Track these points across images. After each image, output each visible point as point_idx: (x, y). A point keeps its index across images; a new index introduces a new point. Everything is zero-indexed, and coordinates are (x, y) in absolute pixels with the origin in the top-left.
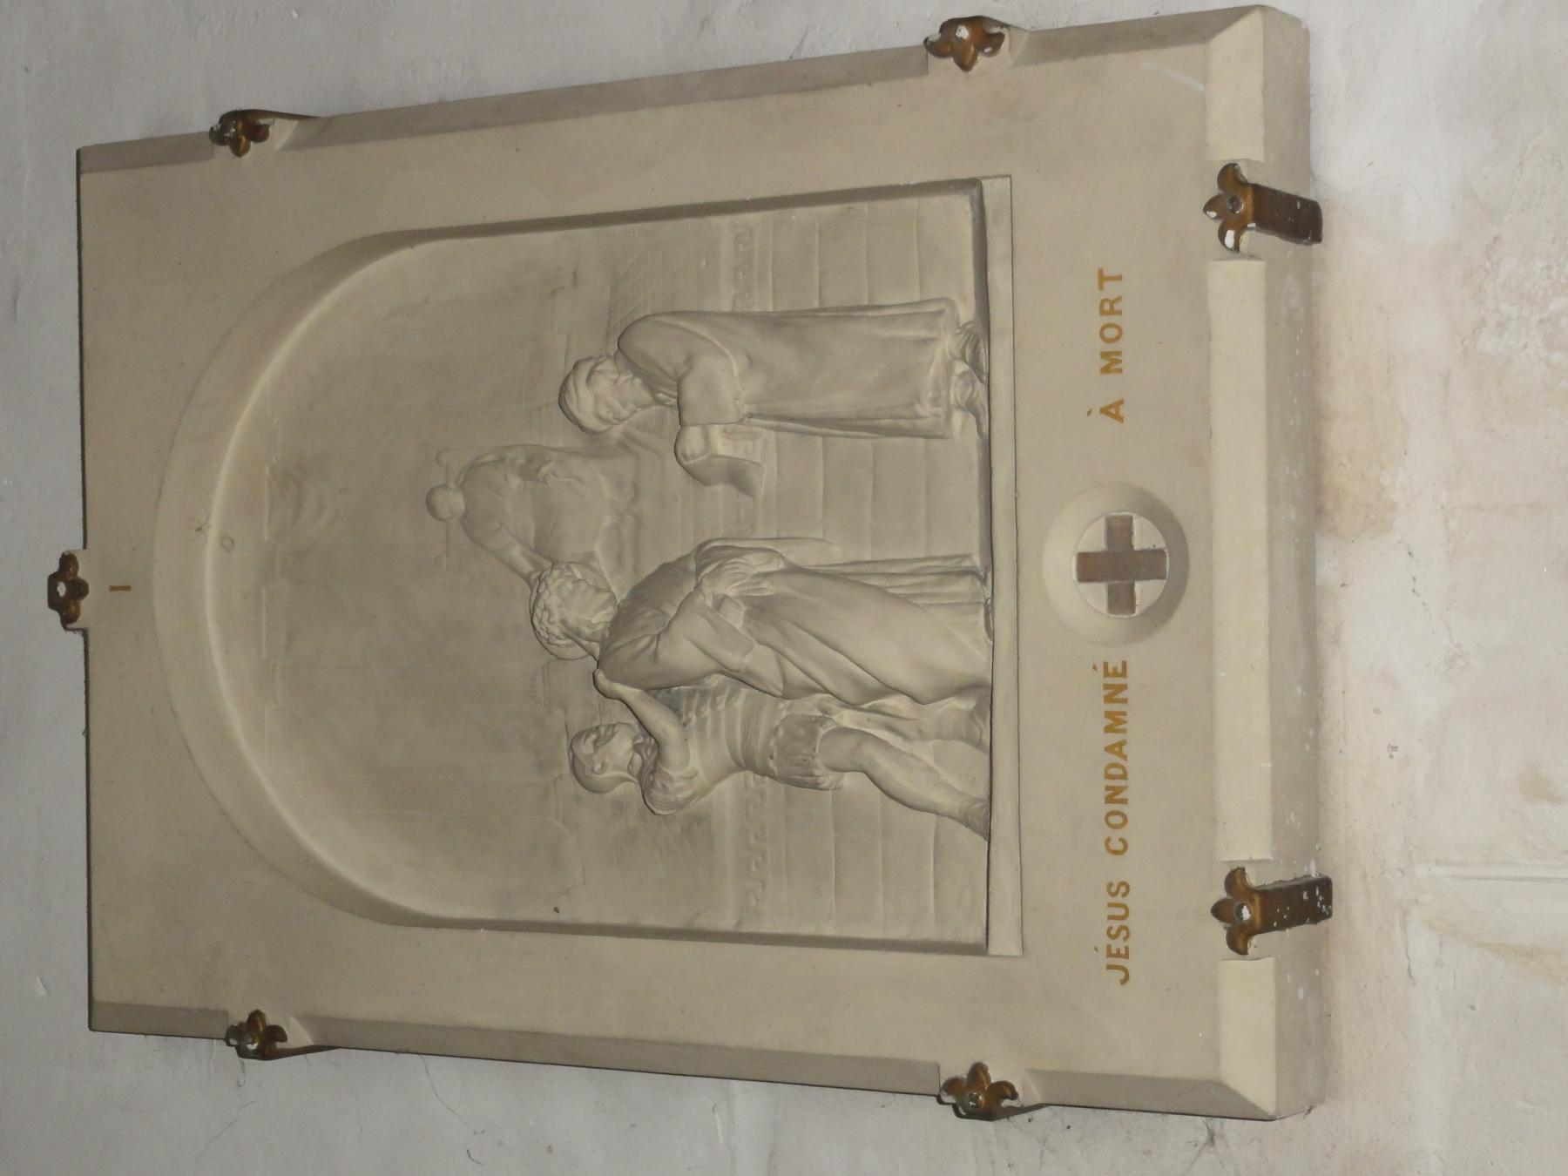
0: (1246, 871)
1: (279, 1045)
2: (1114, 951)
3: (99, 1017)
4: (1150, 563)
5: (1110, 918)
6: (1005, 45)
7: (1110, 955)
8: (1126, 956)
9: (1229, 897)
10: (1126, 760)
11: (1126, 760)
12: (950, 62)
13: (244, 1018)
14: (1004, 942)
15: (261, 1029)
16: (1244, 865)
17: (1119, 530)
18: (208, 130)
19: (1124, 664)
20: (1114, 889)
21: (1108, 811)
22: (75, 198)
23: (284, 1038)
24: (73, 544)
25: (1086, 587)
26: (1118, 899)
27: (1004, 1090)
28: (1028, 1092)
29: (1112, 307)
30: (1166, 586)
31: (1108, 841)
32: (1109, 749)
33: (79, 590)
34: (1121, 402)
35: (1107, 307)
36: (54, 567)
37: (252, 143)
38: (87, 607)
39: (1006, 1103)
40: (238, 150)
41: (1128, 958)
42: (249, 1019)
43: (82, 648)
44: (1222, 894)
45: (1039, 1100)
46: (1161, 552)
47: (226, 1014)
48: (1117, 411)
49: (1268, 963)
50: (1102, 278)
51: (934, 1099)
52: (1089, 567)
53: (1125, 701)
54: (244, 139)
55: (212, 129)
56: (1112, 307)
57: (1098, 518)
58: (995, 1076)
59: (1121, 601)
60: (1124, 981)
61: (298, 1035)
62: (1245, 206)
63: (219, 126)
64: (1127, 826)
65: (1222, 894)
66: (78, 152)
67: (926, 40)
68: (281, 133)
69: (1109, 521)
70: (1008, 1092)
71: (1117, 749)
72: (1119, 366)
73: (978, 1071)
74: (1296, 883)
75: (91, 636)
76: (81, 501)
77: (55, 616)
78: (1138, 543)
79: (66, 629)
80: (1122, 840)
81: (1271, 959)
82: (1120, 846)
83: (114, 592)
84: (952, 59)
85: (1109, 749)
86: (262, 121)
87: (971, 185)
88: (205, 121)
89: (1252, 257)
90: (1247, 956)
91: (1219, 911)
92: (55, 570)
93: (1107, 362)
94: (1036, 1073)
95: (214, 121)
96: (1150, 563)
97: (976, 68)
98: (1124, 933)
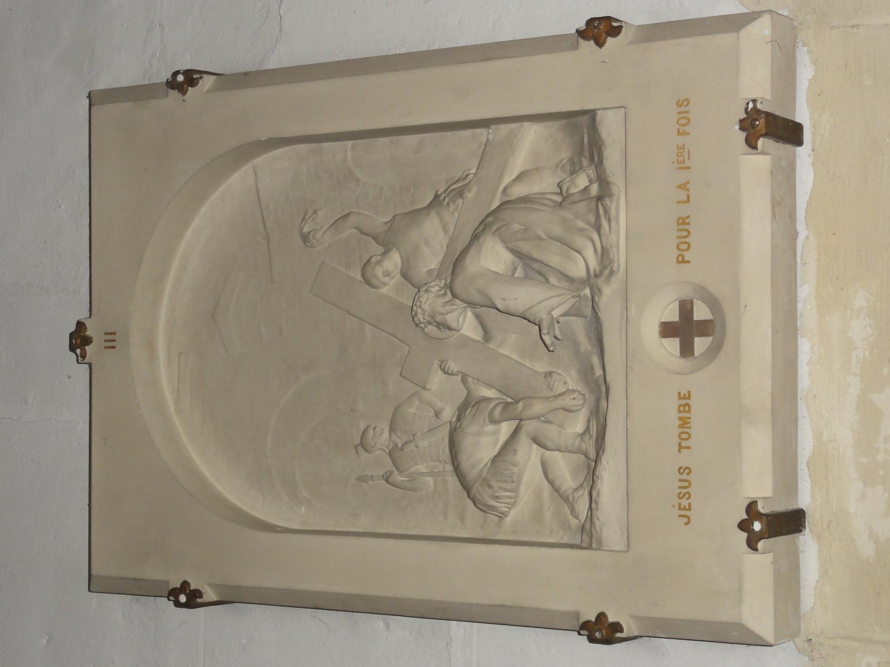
0: (758, 503)
1: (199, 600)
2: (679, 161)
3: (94, 584)
4: (705, 328)
5: (680, 487)
6: (623, 30)
7: (680, 508)
8: (690, 509)
12: (592, 42)
15: (188, 591)
16: (755, 499)
17: (686, 308)
18: (165, 81)
19: (689, 392)
20: (680, 103)
22: (88, 202)
24: (83, 315)
25: (662, 339)
26: (684, 476)
27: (617, 627)
28: (629, 627)
29: (684, 221)
30: (713, 339)
33: (87, 341)
34: (688, 182)
35: (681, 221)
36: (73, 328)
37: (189, 88)
39: (618, 635)
40: (600, 44)
41: (678, 135)
42: (181, 585)
43: (88, 135)
45: (636, 634)
48: (686, 186)
49: (769, 557)
50: (679, 105)
51: (576, 633)
52: (667, 330)
53: (690, 428)
55: (167, 80)
56: (684, 221)
58: (611, 619)
59: (687, 350)
60: (686, 524)
61: (210, 595)
62: (760, 123)
63: (585, 27)
65: (745, 516)
66: (90, 92)
67: (577, 31)
68: (207, 82)
69: (680, 302)
70: (619, 629)
72: (688, 425)
73: (601, 616)
74: (784, 142)
76: (88, 375)
81: (772, 554)
83: (107, 349)
84: (592, 41)
86: (195, 76)
89: (763, 153)
92: (74, 330)
93: (682, 423)
94: (635, 617)
96: (705, 328)
97: (606, 45)
98: (687, 496)
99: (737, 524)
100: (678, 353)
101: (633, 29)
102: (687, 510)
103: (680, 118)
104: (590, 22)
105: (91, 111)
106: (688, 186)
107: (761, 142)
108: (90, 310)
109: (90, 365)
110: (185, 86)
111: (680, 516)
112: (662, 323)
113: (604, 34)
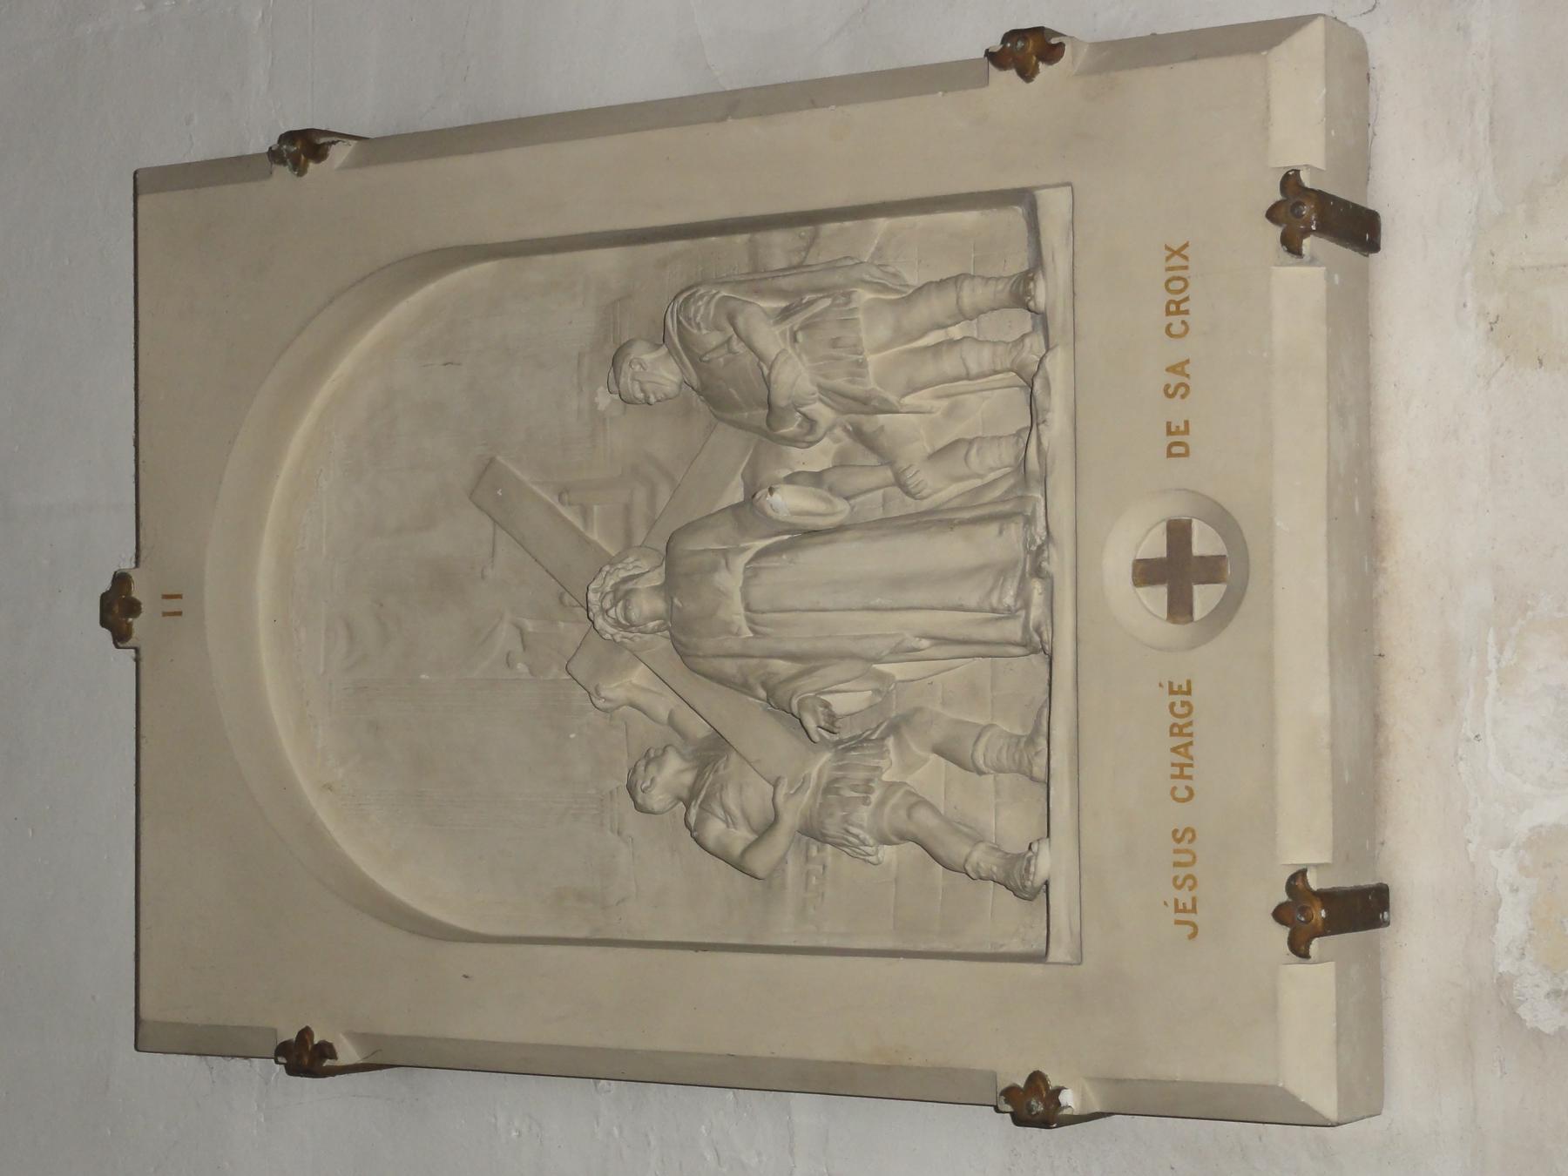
1: (328, 1063)
4: (1212, 569)
5: (1177, 864)
6: (1068, 49)
7: (1177, 910)
9: (1290, 900)
10: (1192, 759)
11: (1192, 759)
13: (293, 1036)
14: (1058, 953)
15: (310, 1047)
16: (1305, 867)
17: (1178, 533)
18: (267, 150)
19: (1187, 423)
21: (1169, 442)
23: (333, 1056)
24: (127, 564)
25: (1141, 591)
29: (1178, 308)
31: (1174, 789)
32: (1174, 750)
36: (105, 584)
38: (138, 624)
40: (1027, 74)
41: (1196, 912)
44: (1284, 897)
45: (1098, 1109)
46: (1223, 557)
47: (275, 1031)
50: (1177, 837)
51: (992, 1108)
52: (1146, 573)
54: (303, 157)
55: (270, 148)
56: (1178, 308)
57: (1158, 523)
59: (1180, 608)
60: (1193, 936)
61: (347, 1053)
63: (1001, 46)
64: (1194, 798)
65: (1284, 897)
66: (135, 173)
68: (339, 154)
71: (1179, 369)
75: (143, 654)
77: (106, 635)
78: (1198, 548)
79: (117, 647)
80: (1184, 322)
82: (1185, 794)
85: (1174, 750)
87: (1024, 198)
88: (262, 141)
89: (1313, 261)
90: (1310, 960)
91: (1280, 914)
95: (274, 141)
96: (1212, 569)
98: (1190, 882)
99: (1265, 213)
100: (1165, 615)
101: (1085, 50)
102: (1189, 911)
103: (1169, 281)
104: (1012, 36)
105: (139, 205)
106: (1192, 751)
107: (1308, 244)
108: (137, 557)
109: (137, 650)
110: (303, 157)
111: (1178, 922)
112: (1139, 561)
113: (1034, 58)
